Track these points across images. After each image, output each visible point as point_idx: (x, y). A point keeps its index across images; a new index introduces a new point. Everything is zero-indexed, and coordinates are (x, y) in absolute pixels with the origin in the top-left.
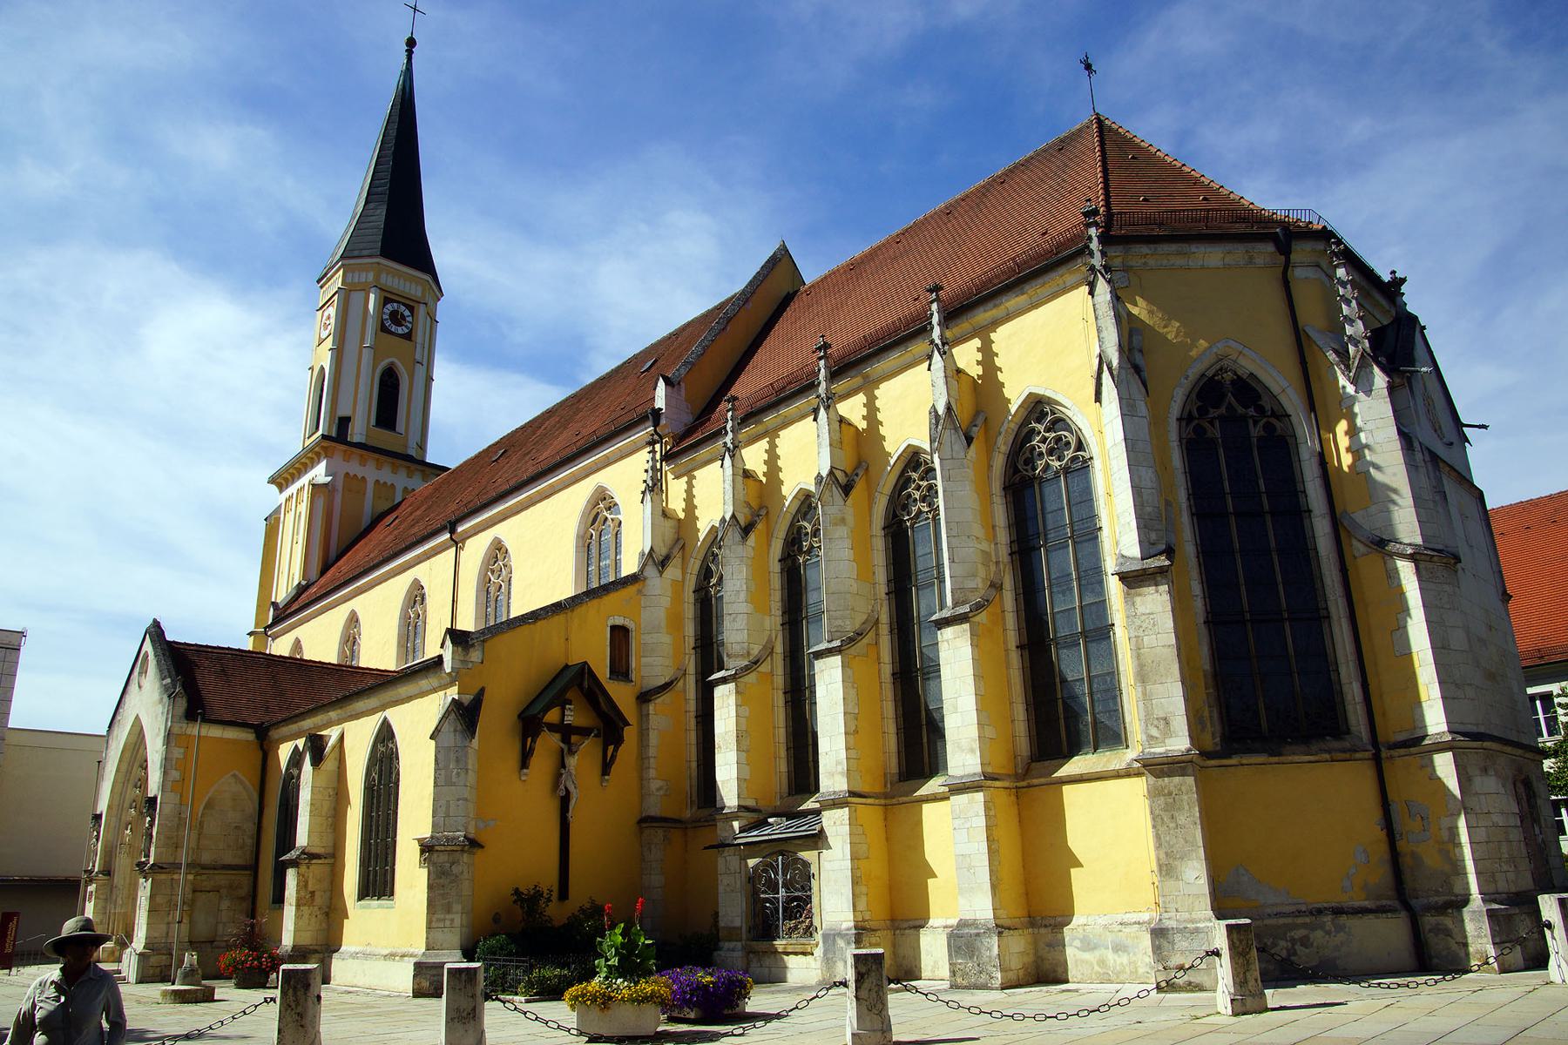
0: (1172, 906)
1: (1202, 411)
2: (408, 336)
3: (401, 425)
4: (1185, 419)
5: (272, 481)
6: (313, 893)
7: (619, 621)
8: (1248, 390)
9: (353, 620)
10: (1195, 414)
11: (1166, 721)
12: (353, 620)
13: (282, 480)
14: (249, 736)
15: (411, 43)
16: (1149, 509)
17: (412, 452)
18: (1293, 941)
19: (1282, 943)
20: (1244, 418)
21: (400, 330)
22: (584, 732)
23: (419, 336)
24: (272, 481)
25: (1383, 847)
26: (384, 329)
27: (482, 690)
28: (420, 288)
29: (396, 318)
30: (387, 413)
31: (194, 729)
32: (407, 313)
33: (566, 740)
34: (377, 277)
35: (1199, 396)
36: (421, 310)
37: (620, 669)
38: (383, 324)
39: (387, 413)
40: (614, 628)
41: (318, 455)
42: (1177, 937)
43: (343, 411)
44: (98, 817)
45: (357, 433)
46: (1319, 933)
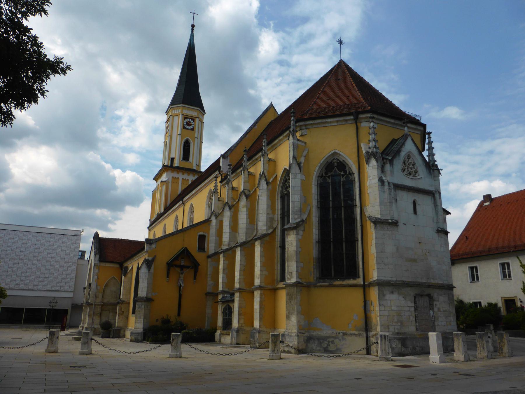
0: (288, 328)
1: (326, 173)
2: (193, 129)
3: (191, 160)
4: (320, 176)
5: (154, 179)
6: (123, 312)
7: (202, 233)
8: (342, 166)
9: (165, 226)
10: (324, 175)
11: (291, 273)
12: (165, 226)
13: (156, 178)
14: (117, 266)
15: (193, 26)
16: (296, 208)
17: (194, 168)
18: (329, 342)
19: (326, 342)
20: (340, 175)
21: (190, 127)
22: (187, 267)
23: (196, 129)
24: (154, 179)
25: (363, 314)
26: (184, 128)
27: (155, 256)
28: (196, 113)
29: (189, 124)
30: (186, 156)
31: (103, 264)
32: (192, 121)
33: (182, 270)
34: (182, 111)
35: (326, 169)
36: (197, 120)
37: (202, 247)
38: (184, 126)
39: (186, 156)
40: (200, 236)
41: (164, 171)
42: (287, 337)
43: (172, 156)
44: (85, 288)
45: (176, 164)
46: (337, 340)
